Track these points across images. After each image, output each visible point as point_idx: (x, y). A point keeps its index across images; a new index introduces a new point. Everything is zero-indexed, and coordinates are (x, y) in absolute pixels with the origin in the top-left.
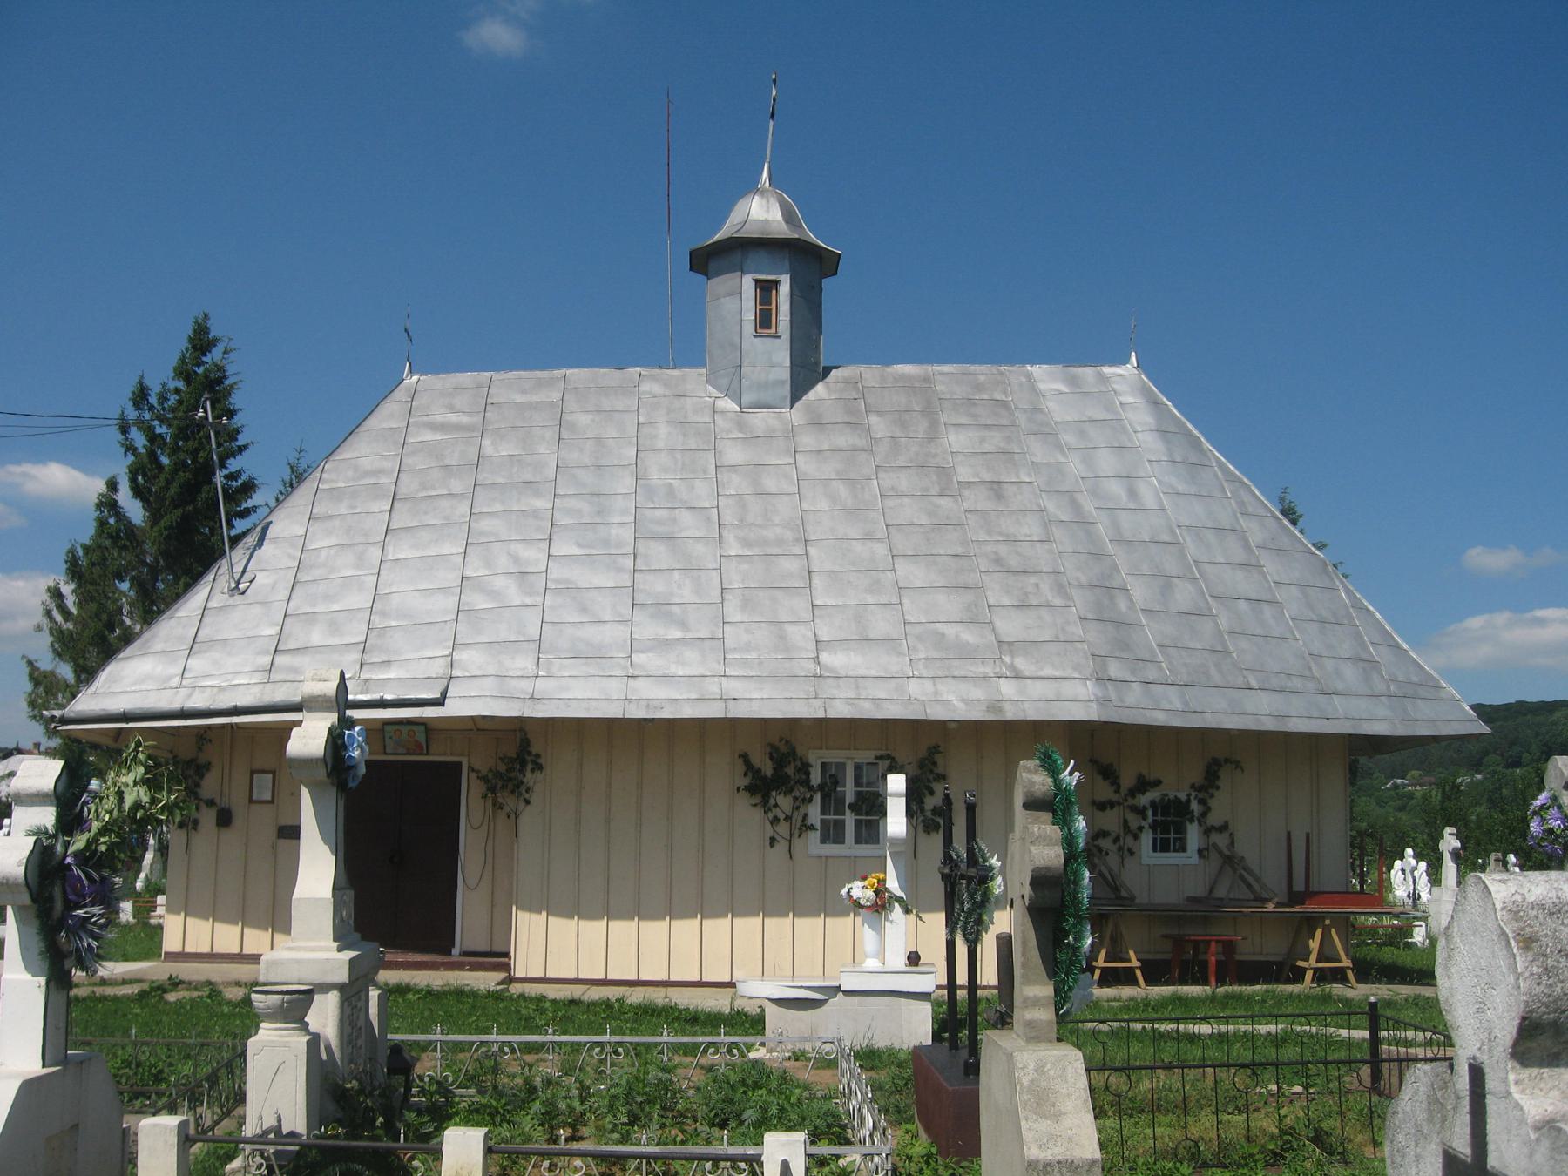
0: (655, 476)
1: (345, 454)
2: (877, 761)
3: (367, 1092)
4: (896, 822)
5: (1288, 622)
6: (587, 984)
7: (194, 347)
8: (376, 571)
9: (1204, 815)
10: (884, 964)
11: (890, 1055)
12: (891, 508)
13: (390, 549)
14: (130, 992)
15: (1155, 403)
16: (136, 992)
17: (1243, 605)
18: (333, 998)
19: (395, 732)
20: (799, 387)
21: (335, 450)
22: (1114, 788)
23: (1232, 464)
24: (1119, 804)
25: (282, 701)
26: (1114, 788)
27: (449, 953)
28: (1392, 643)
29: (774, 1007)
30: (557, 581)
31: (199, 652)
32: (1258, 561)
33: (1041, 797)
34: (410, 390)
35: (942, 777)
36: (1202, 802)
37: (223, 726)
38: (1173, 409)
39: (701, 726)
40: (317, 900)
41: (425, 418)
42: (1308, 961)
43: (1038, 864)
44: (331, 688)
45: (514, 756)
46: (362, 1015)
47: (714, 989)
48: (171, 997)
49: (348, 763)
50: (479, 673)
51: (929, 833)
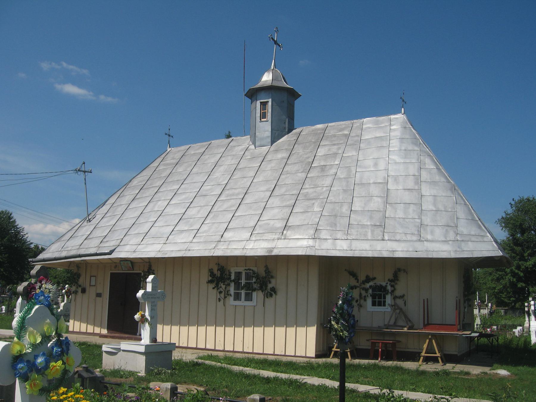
9: (393, 291)
24: (358, 287)
36: (392, 286)
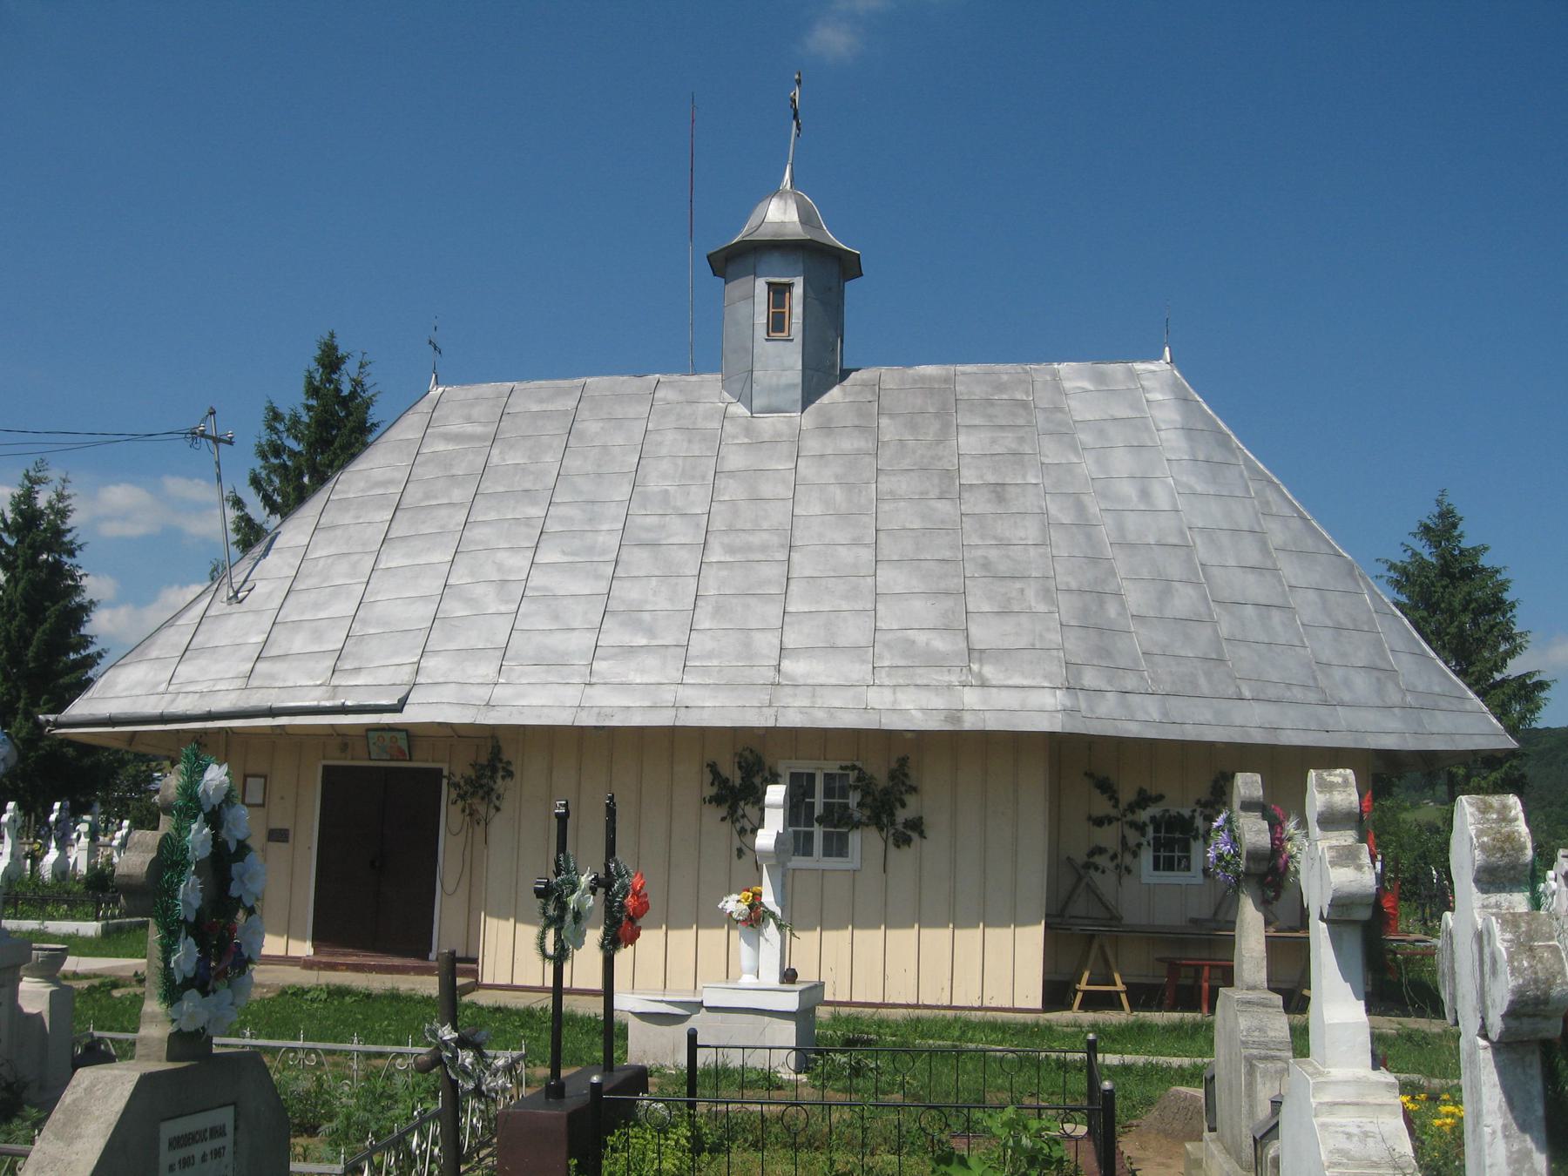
5: (1299, 629)
13: (383, 557)
15: (1185, 400)
16: (86, 986)
17: (1249, 610)
20: (811, 393)
22: (1112, 802)
23: (1261, 462)
24: (1118, 820)
25: (252, 706)
26: (1112, 802)
27: (426, 958)
30: (535, 589)
31: (189, 659)
32: (1275, 563)
38: (1205, 407)
48: (116, 993)
50: (441, 680)
51: (898, 847)
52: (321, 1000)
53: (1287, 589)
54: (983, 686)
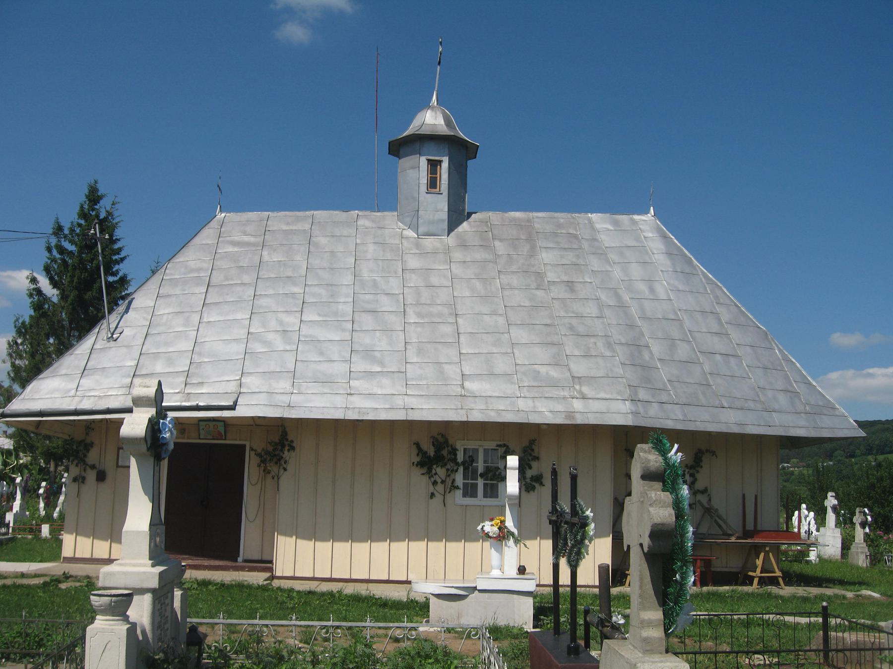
0: (365, 274)
1: (179, 259)
2: (497, 448)
3: (170, 661)
4: (512, 485)
6: (319, 581)
7: (90, 200)
8: (196, 328)
10: (503, 573)
11: (507, 630)
12: (507, 296)
13: (205, 315)
14: (38, 582)
15: (665, 237)
16: (42, 582)
17: (718, 357)
18: (148, 597)
19: (206, 426)
21: (174, 256)
23: (710, 274)
27: (236, 561)
28: (807, 382)
29: (435, 599)
30: (305, 336)
31: (85, 376)
33: (654, 470)
34: (220, 222)
35: (537, 458)
36: (692, 475)
37: (102, 420)
38: (675, 241)
39: (392, 425)
40: (138, 532)
41: (228, 238)
42: (755, 572)
43: (656, 521)
44: (151, 391)
45: (278, 441)
46: (169, 608)
47: (397, 585)
48: (63, 586)
49: (161, 441)
50: (257, 390)
51: (529, 492)
52: (194, 588)
53: (736, 346)
54: (583, 398)
